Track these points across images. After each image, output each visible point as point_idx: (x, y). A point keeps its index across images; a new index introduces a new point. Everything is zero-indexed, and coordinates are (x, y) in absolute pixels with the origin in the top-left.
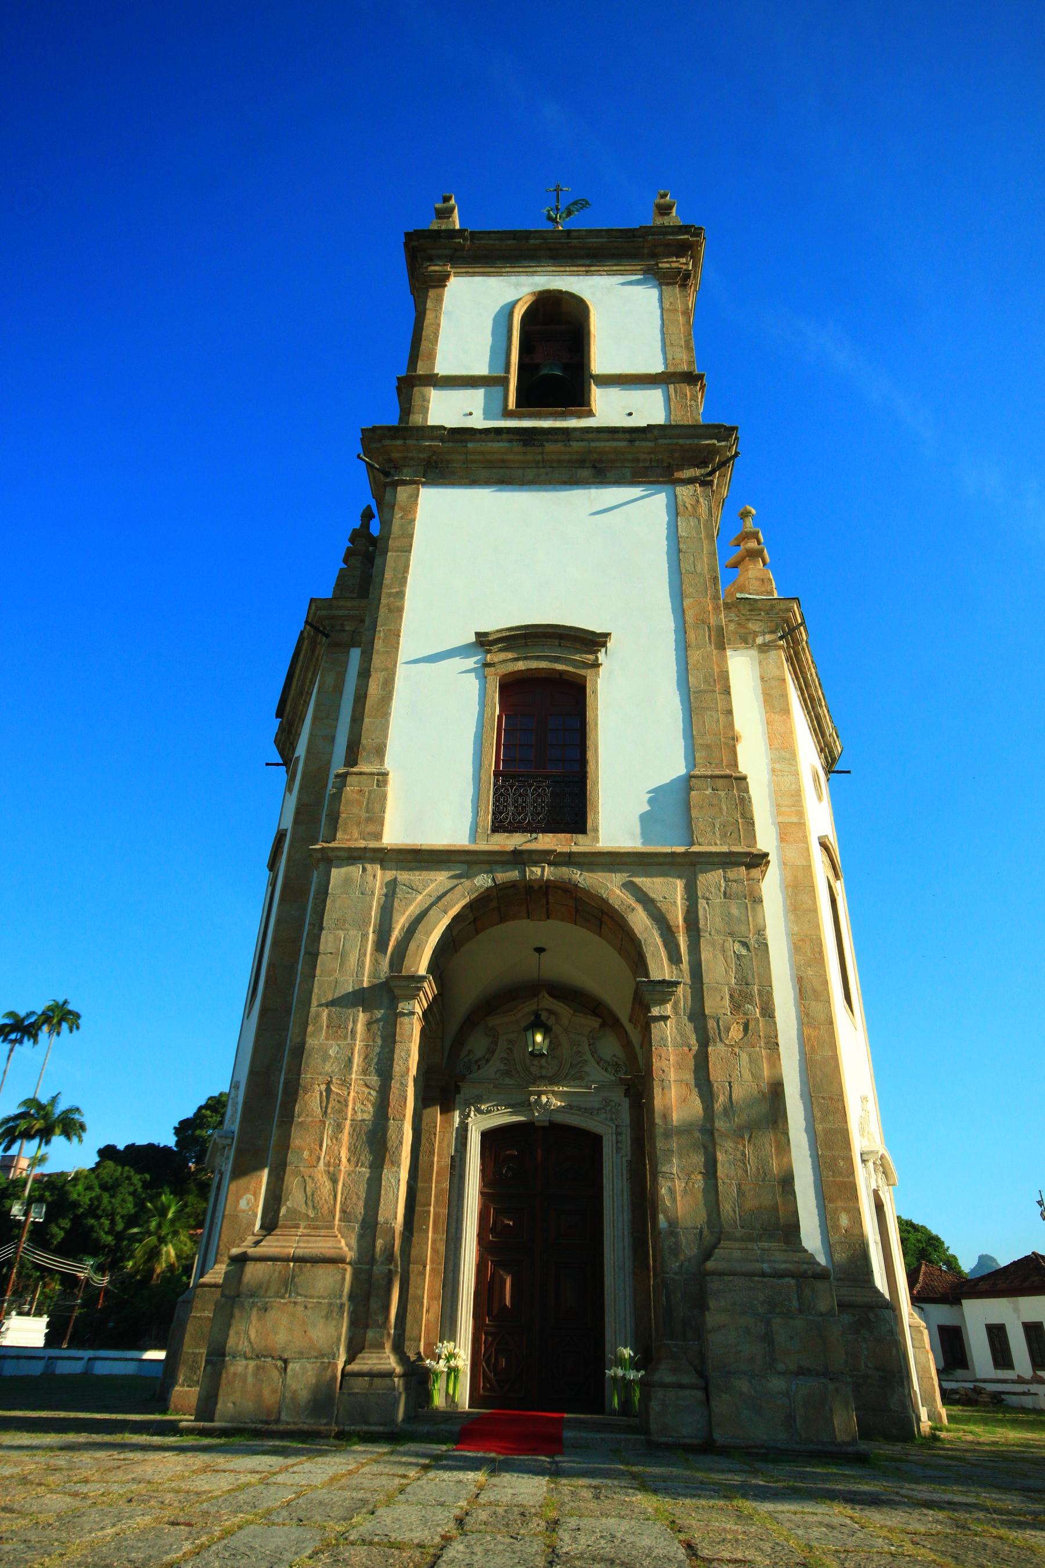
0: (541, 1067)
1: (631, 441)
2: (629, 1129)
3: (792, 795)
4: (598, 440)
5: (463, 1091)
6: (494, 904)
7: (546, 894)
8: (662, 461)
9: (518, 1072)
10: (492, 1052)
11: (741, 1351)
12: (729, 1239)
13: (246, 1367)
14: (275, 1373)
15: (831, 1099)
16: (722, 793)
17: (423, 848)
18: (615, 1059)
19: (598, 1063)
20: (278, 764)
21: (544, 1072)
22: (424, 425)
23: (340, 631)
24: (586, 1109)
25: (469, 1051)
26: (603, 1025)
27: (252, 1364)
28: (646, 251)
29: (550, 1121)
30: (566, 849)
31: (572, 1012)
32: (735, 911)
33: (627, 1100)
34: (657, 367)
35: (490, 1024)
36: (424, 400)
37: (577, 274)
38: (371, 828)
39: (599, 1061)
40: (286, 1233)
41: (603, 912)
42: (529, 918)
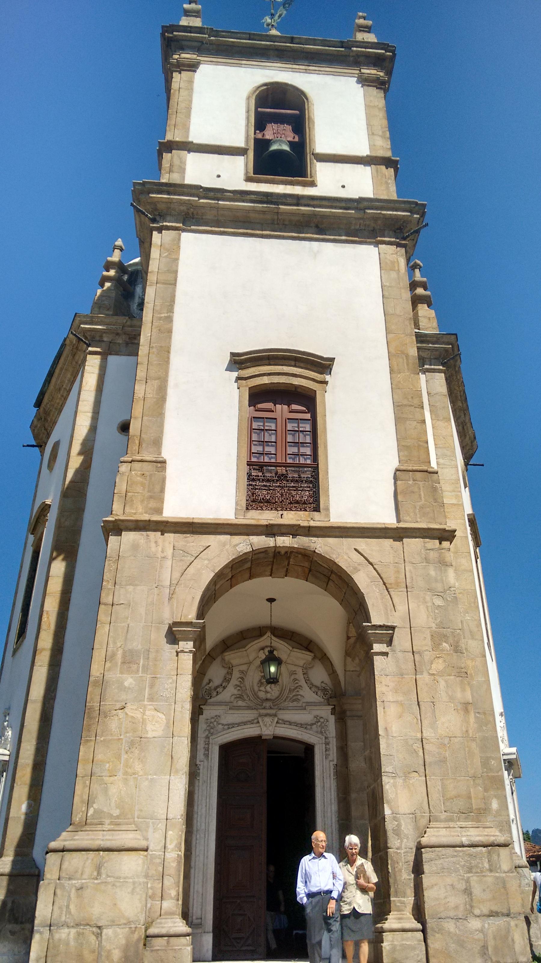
0: (267, 692)
2: (335, 740)
3: (453, 483)
6: (248, 565)
7: (289, 558)
8: (369, 226)
9: (248, 696)
10: (226, 680)
11: (449, 902)
12: (437, 821)
13: (69, 934)
14: (93, 938)
15: (485, 714)
16: (421, 484)
17: (196, 521)
18: (323, 685)
20: (33, 446)
21: (269, 696)
22: (183, 183)
24: (301, 724)
26: (315, 658)
27: (73, 931)
29: (273, 734)
30: (305, 524)
31: (291, 648)
32: (432, 573)
33: (333, 717)
34: (364, 151)
35: (227, 658)
36: (181, 162)
37: (299, 71)
39: (312, 686)
40: (94, 829)
41: (332, 572)
42: (271, 575)
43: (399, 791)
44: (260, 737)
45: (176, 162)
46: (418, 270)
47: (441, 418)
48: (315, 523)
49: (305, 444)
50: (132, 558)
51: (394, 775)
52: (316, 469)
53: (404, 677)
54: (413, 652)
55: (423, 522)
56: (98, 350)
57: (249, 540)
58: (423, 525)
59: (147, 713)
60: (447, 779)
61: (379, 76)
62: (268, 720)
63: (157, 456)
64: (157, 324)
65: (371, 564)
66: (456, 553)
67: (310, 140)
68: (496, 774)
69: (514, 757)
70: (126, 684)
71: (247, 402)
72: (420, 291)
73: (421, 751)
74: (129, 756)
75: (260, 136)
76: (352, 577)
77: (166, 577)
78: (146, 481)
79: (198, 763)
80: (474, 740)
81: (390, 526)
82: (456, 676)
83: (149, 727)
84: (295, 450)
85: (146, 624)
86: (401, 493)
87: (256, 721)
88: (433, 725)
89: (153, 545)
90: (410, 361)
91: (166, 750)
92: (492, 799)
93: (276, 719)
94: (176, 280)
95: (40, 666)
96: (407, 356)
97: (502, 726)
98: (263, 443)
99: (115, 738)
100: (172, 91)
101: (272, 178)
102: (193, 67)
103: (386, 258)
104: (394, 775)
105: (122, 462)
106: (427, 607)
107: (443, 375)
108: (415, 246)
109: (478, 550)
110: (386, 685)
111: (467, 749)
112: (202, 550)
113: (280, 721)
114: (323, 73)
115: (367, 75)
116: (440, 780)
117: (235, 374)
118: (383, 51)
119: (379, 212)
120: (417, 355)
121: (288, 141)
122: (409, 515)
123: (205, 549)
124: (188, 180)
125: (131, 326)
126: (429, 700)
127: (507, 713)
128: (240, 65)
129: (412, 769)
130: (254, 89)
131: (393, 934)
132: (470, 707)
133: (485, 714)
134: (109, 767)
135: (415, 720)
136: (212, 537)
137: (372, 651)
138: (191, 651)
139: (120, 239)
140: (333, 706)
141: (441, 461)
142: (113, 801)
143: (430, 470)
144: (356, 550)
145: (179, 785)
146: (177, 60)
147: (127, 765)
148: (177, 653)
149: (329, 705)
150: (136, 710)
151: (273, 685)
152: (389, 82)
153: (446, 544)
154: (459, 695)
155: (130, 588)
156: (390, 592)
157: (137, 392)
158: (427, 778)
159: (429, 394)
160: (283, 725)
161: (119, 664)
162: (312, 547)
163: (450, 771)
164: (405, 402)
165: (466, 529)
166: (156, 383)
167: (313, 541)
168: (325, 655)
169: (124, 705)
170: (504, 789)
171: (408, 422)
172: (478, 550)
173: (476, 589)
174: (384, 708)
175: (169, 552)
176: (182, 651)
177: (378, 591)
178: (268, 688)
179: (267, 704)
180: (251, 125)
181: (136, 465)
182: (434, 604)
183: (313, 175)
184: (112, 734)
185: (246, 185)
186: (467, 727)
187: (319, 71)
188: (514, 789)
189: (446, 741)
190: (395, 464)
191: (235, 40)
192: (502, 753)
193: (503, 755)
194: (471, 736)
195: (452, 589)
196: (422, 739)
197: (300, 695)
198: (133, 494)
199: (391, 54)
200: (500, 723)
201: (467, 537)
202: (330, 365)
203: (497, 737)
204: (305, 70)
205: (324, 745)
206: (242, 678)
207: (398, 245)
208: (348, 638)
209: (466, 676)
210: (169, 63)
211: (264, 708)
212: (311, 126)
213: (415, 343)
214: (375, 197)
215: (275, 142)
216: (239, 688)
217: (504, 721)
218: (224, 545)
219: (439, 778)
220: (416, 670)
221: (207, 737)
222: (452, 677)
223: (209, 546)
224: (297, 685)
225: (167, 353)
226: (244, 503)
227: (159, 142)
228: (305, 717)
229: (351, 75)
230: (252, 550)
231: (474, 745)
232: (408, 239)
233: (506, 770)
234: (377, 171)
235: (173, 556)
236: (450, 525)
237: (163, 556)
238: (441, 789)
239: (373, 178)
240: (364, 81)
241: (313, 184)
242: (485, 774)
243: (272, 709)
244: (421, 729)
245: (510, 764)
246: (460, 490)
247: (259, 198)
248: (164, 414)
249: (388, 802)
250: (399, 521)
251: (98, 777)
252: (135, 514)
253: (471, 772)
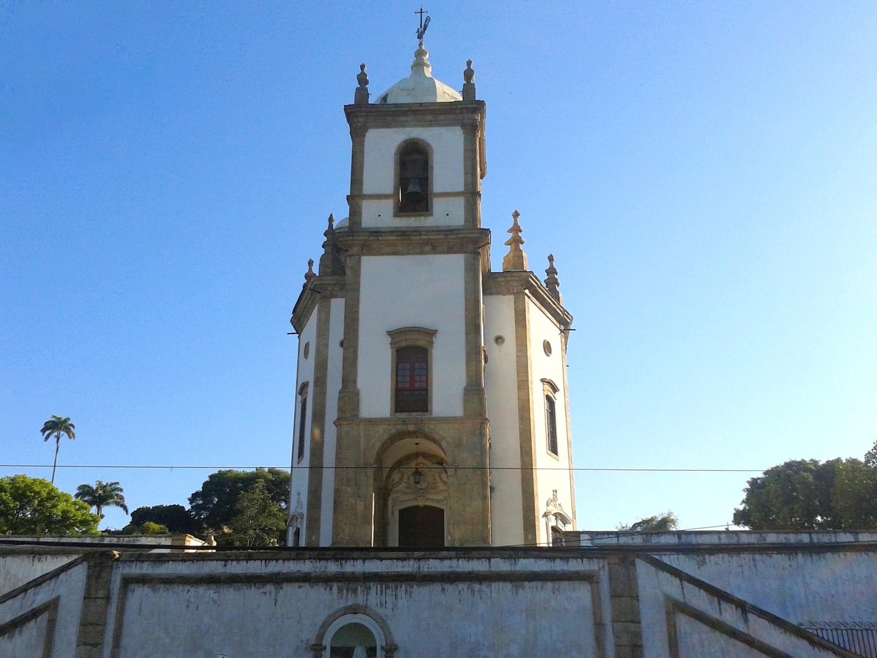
1: (447, 235)
4: (432, 235)
5: (391, 495)
10: (401, 479)
19: (442, 483)
21: (422, 487)
23: (325, 290)
25: (393, 480)
28: (458, 111)
34: (461, 188)
56: (530, 279)
93: (425, 498)
125: (342, 281)
131: (449, 524)
157: (403, 601)
179: (421, 491)
221: (393, 507)
226: (394, 409)
247: (400, 233)
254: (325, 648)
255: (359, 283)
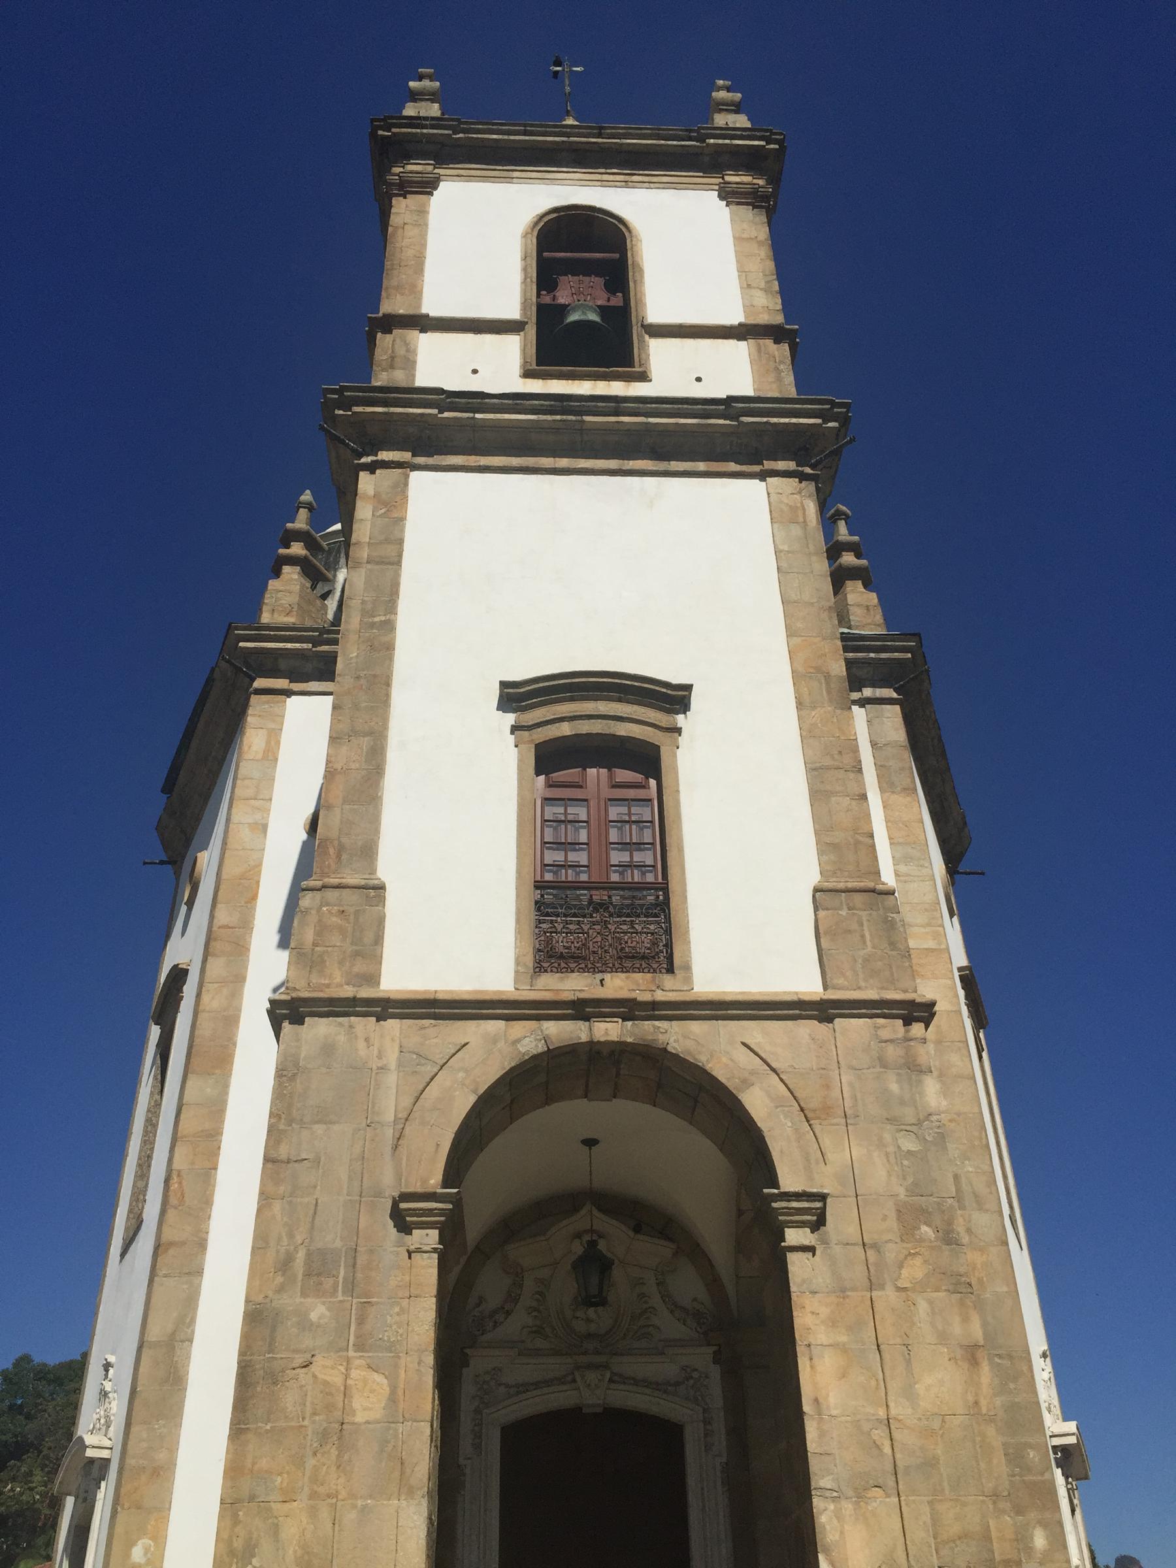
0: (589, 1320)
2: (722, 1414)
3: (926, 910)
15: (1010, 1357)
16: (864, 915)
19: (672, 1312)
20: (162, 863)
24: (657, 1384)
30: (645, 997)
32: (894, 1087)
34: (734, 316)
36: (408, 351)
38: (360, 967)
43: (846, 1527)
44: (576, 1411)
45: (401, 351)
46: (843, 521)
47: (899, 789)
48: (666, 996)
49: (642, 846)
50: (324, 1070)
51: (835, 1494)
52: (665, 888)
53: (848, 1296)
54: (864, 1245)
55: (872, 989)
57: (542, 1031)
58: (871, 994)
59: (354, 1373)
60: (941, 1500)
61: (757, 186)
62: (592, 1376)
63: (367, 877)
64: (367, 635)
65: (774, 1070)
66: (939, 1042)
67: (636, 303)
68: (1040, 1478)
69: (1072, 1440)
70: (314, 1316)
71: (531, 770)
72: (848, 559)
73: (887, 1443)
74: (318, 1461)
75: (547, 299)
76: (739, 1097)
77: (389, 1106)
78: (349, 923)
79: (462, 1461)
80: (991, 1419)
81: (806, 998)
82: (949, 1291)
83: (357, 1403)
84: (624, 857)
85: (349, 1198)
86: (826, 933)
87: (569, 1378)
88: (909, 1393)
89: (361, 1044)
90: (832, 686)
91: (390, 1448)
92: (1034, 1528)
93: (608, 1375)
94: (400, 555)
95: (165, 1276)
96: (828, 677)
97: (1047, 1379)
98: (558, 845)
99: (293, 1424)
100: (390, 229)
101: (569, 371)
102: (428, 186)
103: (781, 502)
104: (835, 1494)
105: (304, 890)
106: (887, 1155)
107: (897, 708)
108: (833, 477)
109: (981, 1035)
110: (813, 1313)
111: (978, 1439)
112: (453, 1051)
113: (616, 1378)
114: (657, 185)
115: (735, 186)
116: (928, 1502)
117: (510, 718)
118: (762, 143)
119: (765, 420)
120: (845, 674)
121: (598, 306)
122: (843, 974)
123: (459, 1050)
124: (419, 383)
126: (898, 1341)
127: (1056, 1352)
128: (509, 180)
129: (871, 1482)
130: (535, 219)
132: (980, 1354)
133: (1010, 1357)
134: (281, 1482)
135: (873, 1383)
136: (471, 1025)
137: (783, 1244)
138: (435, 1250)
139: (308, 492)
140: (715, 1348)
141: (902, 868)
142: (291, 1552)
143: (880, 887)
144: (744, 1044)
145: (415, 1518)
146: (399, 176)
147: (314, 1479)
148: (410, 1253)
149: (709, 1345)
150: (333, 1368)
151: (600, 1309)
152: (774, 195)
153: (917, 1029)
154: (957, 1329)
155: (319, 1129)
156: (814, 1126)
158: (902, 1499)
159: (874, 744)
160: (622, 1387)
161: (300, 1277)
162: (661, 1042)
163: (945, 1484)
164: (828, 762)
165: (957, 996)
166: (366, 742)
167: (662, 1030)
168: (698, 1245)
169: (310, 1359)
170: (1057, 1508)
171: (833, 799)
172: (981, 1035)
173: (981, 1113)
174: (811, 1359)
175: (392, 1057)
176: (419, 1251)
177: (790, 1124)
178: (591, 1312)
180: (532, 281)
181: (332, 895)
182: (899, 1147)
183: (643, 362)
184: (286, 1417)
185: (524, 384)
186: (977, 1395)
187: (649, 182)
188: (1076, 1501)
189: (936, 1424)
190: (814, 877)
191: (500, 137)
192: (1048, 1433)
193: (1051, 1437)
194: (984, 1411)
195: (934, 1118)
196: (888, 1420)
197: (653, 1326)
198: (325, 949)
199: (777, 146)
200: (1043, 1371)
201: (960, 1012)
202: (684, 696)
203: (1038, 1403)
204: (624, 183)
205: (702, 1425)
206: (541, 1293)
207: (802, 477)
208: (740, 1213)
209: (969, 1290)
210: (386, 182)
211: (585, 1353)
212: (638, 278)
213: (842, 652)
214: (757, 395)
215: (575, 309)
216: (535, 1314)
217: (1049, 1368)
218: (495, 1040)
219: (926, 1498)
220: (870, 1280)
221: (478, 1411)
222: (942, 1294)
223: (467, 1043)
224: (645, 1306)
225: (384, 687)
226: (529, 960)
227: (368, 317)
228: (668, 1369)
229: (706, 187)
230: (546, 1049)
231: (991, 1431)
232: (821, 466)
233: (1057, 1468)
234: (759, 350)
235: (400, 1064)
236: (926, 991)
237: (379, 1065)
238: (929, 1521)
239: (753, 362)
240: (728, 195)
241: (643, 377)
242: (1017, 1478)
243: (600, 1354)
244: (886, 1399)
245: (1067, 1457)
246: (940, 922)
248: (381, 798)
249: (827, 1552)
250: (825, 987)
251: (261, 1504)
252: (328, 986)
253: (989, 1486)
254: (376, 456)
255: (400, 542)
